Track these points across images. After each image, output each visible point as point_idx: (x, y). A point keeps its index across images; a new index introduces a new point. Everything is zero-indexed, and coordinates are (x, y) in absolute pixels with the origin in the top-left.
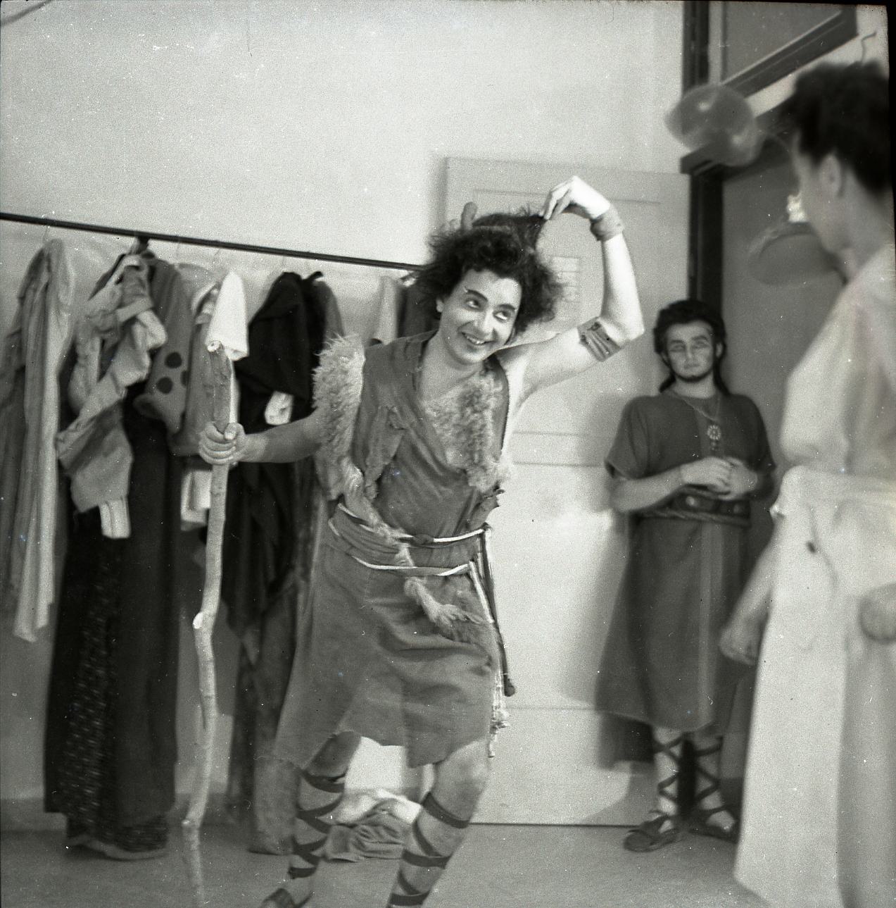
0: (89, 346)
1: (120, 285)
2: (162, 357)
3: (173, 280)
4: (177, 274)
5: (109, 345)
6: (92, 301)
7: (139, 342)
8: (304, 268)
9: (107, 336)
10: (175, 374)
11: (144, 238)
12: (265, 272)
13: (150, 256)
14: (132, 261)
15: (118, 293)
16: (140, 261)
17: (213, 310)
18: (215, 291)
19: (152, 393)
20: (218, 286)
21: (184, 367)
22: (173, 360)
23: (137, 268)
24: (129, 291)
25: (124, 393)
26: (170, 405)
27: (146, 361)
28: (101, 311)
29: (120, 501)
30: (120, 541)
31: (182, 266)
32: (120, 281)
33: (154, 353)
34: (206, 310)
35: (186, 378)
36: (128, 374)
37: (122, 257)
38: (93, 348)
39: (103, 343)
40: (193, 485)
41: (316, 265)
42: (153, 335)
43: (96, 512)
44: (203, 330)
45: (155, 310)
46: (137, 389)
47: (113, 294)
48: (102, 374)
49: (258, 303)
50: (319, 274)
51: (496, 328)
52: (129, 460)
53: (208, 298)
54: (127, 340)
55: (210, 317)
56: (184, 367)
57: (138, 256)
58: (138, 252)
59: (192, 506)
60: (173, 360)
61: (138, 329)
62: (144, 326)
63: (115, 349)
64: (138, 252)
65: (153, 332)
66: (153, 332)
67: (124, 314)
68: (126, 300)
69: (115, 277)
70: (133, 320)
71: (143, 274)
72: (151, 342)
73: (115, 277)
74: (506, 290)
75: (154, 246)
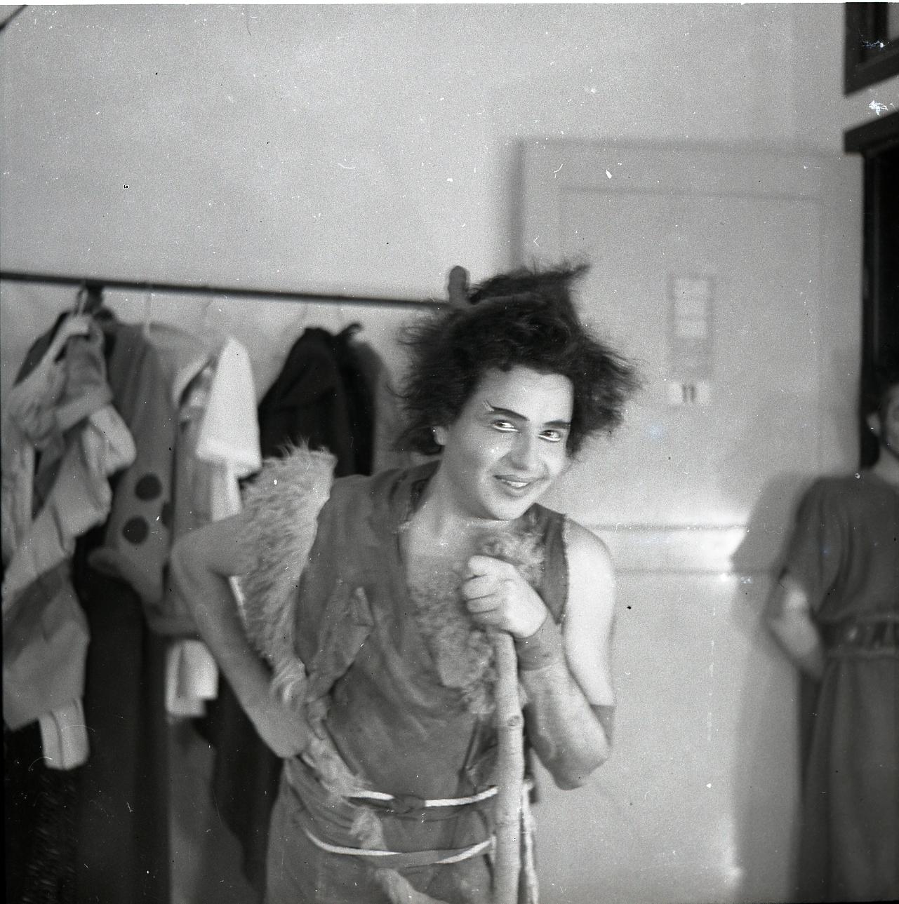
0: (17, 458)
1: (62, 364)
2: (130, 482)
3: (144, 354)
4: (146, 348)
5: (47, 460)
6: (19, 388)
7: (93, 464)
8: (331, 319)
9: (45, 444)
10: (151, 512)
11: (94, 287)
12: (281, 323)
13: (106, 315)
14: (77, 325)
15: (59, 377)
16: (90, 328)
17: (206, 399)
18: (207, 372)
19: (115, 546)
20: (213, 363)
21: (164, 496)
22: (147, 488)
23: (87, 337)
24: (75, 375)
25: (70, 547)
26: (137, 562)
27: (105, 493)
28: (32, 406)
29: (73, 708)
30: (78, 771)
31: (155, 327)
32: (61, 356)
33: (115, 479)
34: (196, 400)
35: (168, 514)
36: (80, 511)
37: (63, 318)
38: (22, 463)
39: (38, 456)
40: (183, 662)
41: (351, 313)
42: (112, 449)
43: (33, 731)
44: (192, 427)
45: (118, 404)
46: (92, 539)
47: (50, 378)
48: (39, 503)
49: (271, 372)
50: (356, 326)
51: (593, 271)
52: (83, 639)
53: (196, 382)
54: (74, 451)
55: (201, 412)
56: (164, 496)
57: (88, 318)
58: (88, 310)
59: (182, 691)
60: (147, 488)
61: (91, 440)
62: (100, 434)
63: (56, 466)
64: (88, 310)
65: (112, 443)
66: (112, 443)
67: (68, 416)
68: (71, 390)
69: (53, 351)
70: (83, 423)
71: (97, 346)
72: (112, 463)
73: (53, 351)
74: (542, 396)
75: (111, 298)
